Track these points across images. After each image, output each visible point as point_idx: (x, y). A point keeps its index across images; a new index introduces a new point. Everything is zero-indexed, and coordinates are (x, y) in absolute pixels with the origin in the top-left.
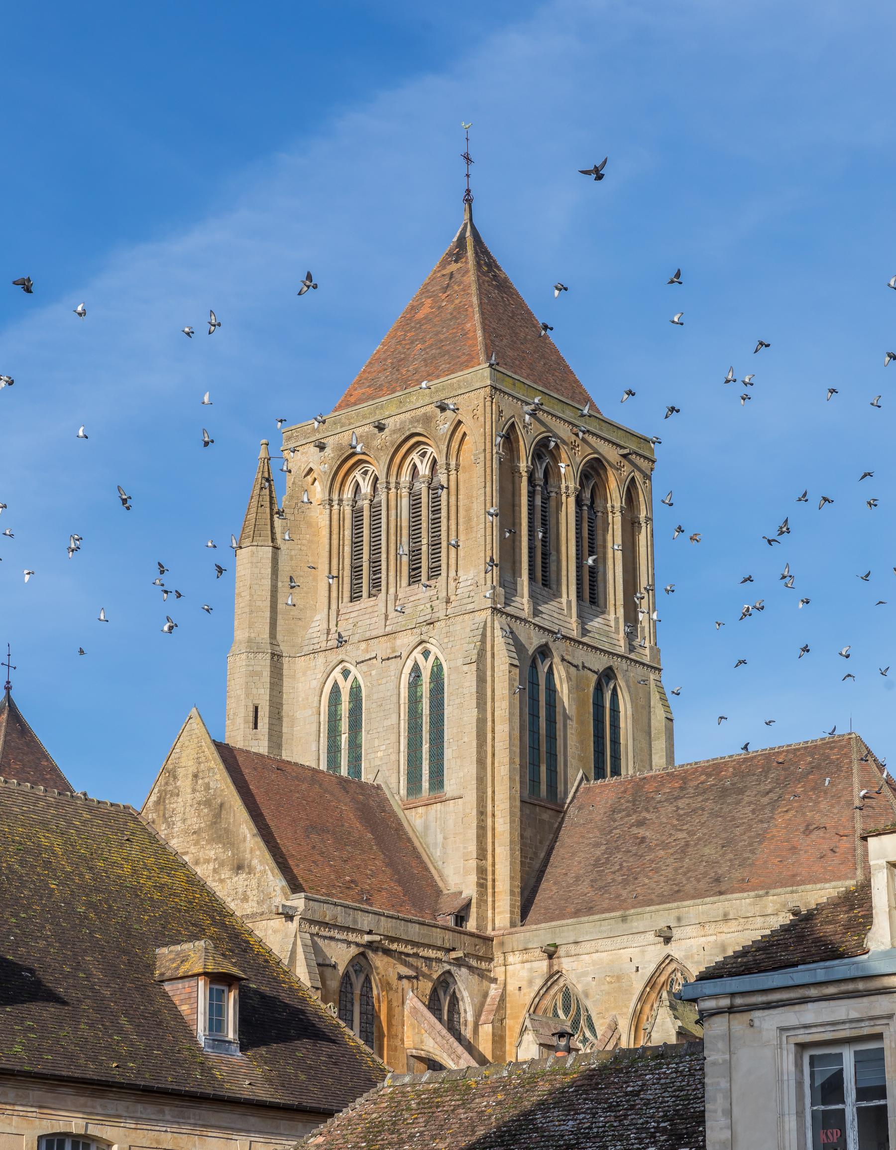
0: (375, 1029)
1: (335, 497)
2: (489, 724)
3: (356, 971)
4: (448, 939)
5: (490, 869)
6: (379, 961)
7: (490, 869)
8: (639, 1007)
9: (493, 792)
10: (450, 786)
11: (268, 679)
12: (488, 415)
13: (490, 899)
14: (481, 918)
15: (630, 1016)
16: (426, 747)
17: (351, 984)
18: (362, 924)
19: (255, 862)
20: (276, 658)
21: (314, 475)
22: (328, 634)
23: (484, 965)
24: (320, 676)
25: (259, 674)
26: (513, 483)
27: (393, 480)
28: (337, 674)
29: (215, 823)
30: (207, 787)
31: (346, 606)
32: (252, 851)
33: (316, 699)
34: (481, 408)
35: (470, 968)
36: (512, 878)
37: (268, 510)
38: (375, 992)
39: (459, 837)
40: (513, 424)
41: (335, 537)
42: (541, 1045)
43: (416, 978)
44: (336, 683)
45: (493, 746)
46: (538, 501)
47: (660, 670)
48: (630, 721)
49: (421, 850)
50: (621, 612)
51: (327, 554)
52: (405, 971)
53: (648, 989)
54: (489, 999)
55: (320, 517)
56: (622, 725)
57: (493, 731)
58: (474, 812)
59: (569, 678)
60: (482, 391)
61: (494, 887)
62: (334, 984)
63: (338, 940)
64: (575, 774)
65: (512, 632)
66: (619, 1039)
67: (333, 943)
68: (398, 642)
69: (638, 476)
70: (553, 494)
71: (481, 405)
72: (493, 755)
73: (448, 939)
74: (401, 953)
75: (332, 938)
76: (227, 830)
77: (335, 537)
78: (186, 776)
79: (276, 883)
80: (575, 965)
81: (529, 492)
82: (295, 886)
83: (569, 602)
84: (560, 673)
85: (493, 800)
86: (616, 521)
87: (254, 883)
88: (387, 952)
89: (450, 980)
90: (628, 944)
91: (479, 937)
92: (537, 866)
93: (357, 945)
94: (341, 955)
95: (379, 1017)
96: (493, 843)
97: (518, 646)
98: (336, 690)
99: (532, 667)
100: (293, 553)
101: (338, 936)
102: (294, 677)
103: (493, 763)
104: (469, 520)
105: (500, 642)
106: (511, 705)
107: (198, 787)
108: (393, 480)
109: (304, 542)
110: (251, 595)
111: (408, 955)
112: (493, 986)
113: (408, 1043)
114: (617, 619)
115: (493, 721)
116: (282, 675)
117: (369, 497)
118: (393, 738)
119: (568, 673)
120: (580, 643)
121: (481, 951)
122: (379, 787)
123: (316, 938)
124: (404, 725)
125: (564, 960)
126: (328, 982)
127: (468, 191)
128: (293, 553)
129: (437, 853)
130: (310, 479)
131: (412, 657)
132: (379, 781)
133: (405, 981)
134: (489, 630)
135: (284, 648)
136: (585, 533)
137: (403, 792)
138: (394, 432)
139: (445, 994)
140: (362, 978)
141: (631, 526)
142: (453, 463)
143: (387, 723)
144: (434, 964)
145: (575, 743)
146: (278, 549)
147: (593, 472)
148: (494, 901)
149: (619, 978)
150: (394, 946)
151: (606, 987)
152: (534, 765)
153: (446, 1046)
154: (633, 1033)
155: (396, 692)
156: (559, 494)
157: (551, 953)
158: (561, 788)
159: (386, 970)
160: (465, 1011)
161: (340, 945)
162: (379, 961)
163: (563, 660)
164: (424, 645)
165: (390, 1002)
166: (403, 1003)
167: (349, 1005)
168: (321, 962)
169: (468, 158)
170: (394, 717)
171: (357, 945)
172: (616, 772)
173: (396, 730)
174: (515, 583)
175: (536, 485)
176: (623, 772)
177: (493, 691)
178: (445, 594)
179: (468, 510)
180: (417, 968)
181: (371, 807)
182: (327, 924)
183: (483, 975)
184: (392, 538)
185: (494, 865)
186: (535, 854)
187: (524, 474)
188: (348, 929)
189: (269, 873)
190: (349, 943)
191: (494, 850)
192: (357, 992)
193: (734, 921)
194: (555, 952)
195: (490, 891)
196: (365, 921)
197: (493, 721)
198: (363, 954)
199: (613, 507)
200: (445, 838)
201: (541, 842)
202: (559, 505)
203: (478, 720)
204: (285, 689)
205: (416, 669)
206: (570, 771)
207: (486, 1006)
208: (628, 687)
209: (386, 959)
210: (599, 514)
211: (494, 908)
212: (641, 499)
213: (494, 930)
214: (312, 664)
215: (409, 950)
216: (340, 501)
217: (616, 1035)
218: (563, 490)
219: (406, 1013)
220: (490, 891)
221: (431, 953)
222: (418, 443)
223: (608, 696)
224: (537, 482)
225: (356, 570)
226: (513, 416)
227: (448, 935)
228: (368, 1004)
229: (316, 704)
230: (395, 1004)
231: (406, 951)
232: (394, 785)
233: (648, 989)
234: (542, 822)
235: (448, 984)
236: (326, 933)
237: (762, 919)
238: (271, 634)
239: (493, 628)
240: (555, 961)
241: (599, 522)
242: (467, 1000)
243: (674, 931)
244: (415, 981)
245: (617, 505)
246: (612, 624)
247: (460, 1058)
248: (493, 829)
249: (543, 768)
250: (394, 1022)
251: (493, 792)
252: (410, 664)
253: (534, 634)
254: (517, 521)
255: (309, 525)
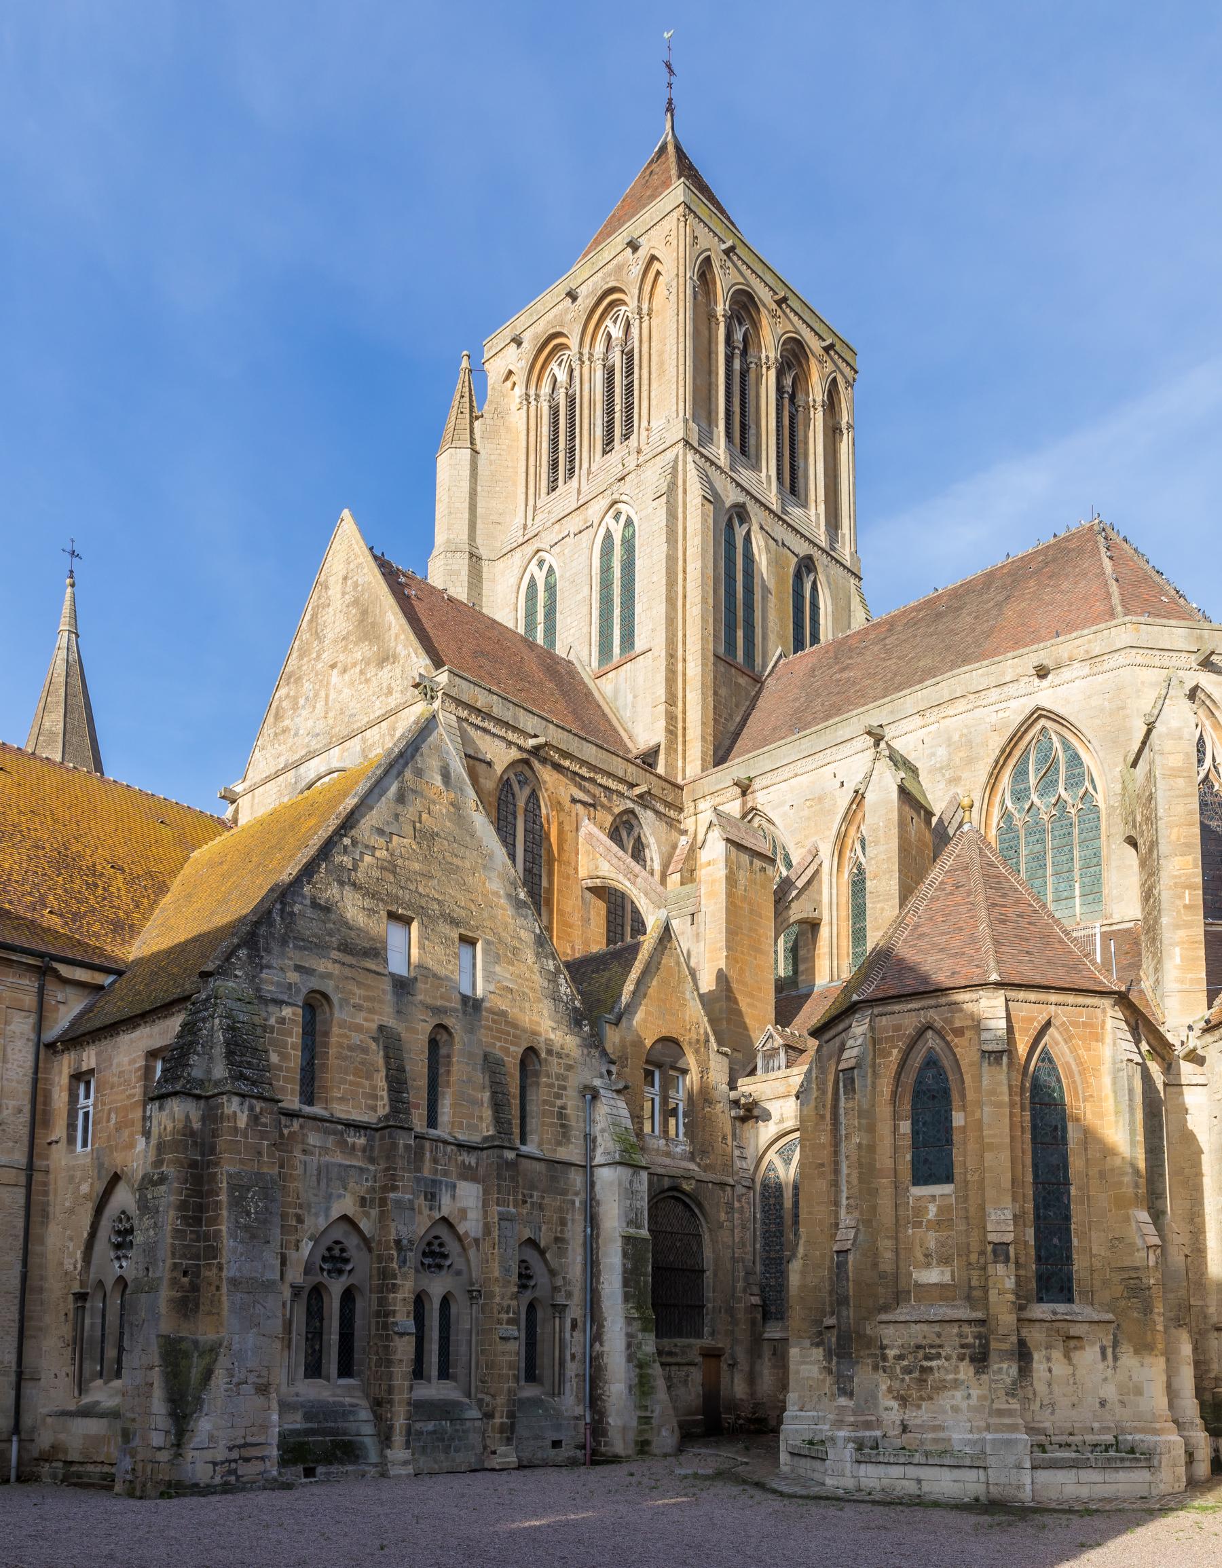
0: (543, 852)
1: (532, 392)
2: (680, 563)
3: (519, 782)
4: (632, 773)
5: (680, 716)
6: (547, 775)
7: (680, 716)
8: (843, 828)
9: (685, 635)
10: (640, 644)
11: (466, 578)
12: (682, 237)
13: (680, 748)
14: (670, 765)
15: (833, 839)
16: (617, 612)
17: (513, 795)
18: (525, 724)
19: (400, 648)
20: (474, 559)
21: (513, 378)
22: (525, 529)
23: (672, 814)
24: (517, 572)
25: (458, 573)
26: (710, 329)
27: (586, 351)
28: (533, 567)
29: (362, 621)
30: (356, 585)
31: (544, 498)
32: (397, 636)
33: (514, 595)
34: (674, 233)
35: (657, 812)
36: (703, 723)
37: (468, 416)
38: (544, 811)
39: (648, 695)
40: (708, 258)
41: (532, 433)
42: (728, 840)
43: (593, 806)
44: (532, 576)
45: (685, 587)
46: (737, 365)
47: (861, 579)
48: (830, 618)
49: (611, 716)
50: (822, 508)
51: (524, 451)
52: (580, 795)
53: (854, 806)
54: (678, 852)
55: (518, 419)
56: (822, 621)
57: (685, 572)
58: (664, 653)
59: (768, 551)
60: (675, 214)
61: (684, 736)
62: (489, 784)
63: (494, 735)
64: (774, 646)
65: (707, 476)
66: (820, 865)
67: (488, 738)
68: (590, 511)
69: (840, 380)
70: (753, 365)
71: (674, 228)
72: (685, 597)
73: (632, 773)
74: (575, 773)
75: (485, 730)
76: (373, 625)
77: (532, 433)
78: (337, 582)
79: (419, 663)
80: (770, 798)
81: (726, 354)
82: (438, 663)
83: (768, 477)
84: (758, 543)
85: (684, 643)
86: (818, 418)
87: (398, 671)
88: (557, 767)
89: (634, 822)
90: (832, 759)
91: (666, 780)
92: (732, 729)
93: (520, 748)
94: (500, 755)
95: (548, 838)
96: (684, 689)
97: (712, 498)
98: (532, 584)
99: (729, 522)
100: (492, 457)
101: (494, 730)
102: (493, 580)
103: (684, 605)
104: (661, 363)
105: (692, 473)
106: (704, 541)
107: (348, 590)
108: (586, 351)
109: (504, 447)
110: (450, 497)
111: (583, 778)
112: (683, 838)
113: (583, 872)
114: (817, 515)
115: (685, 561)
116: (481, 577)
117: (565, 385)
118: (585, 610)
119: (766, 543)
120: (780, 518)
121: (667, 800)
122: (569, 662)
123: (465, 725)
124: (596, 596)
125: (757, 794)
126: (482, 780)
127: (670, 100)
128: (492, 457)
129: (626, 714)
130: (509, 384)
131: (604, 524)
132: (572, 657)
133: (579, 806)
134: (680, 464)
135: (483, 552)
136: (786, 422)
137: (595, 664)
138: (587, 297)
139: (628, 835)
140: (527, 791)
141: (833, 432)
142: (645, 307)
143: (579, 597)
144: (615, 797)
145: (774, 619)
146: (477, 452)
147: (794, 356)
148: (684, 751)
149: (820, 799)
150: (566, 763)
151: (806, 813)
152: (731, 628)
153: (623, 867)
154: (836, 859)
155: (588, 562)
156: (759, 366)
157: (745, 788)
158: (758, 660)
159: (556, 788)
160: (652, 859)
161: (497, 741)
162: (547, 775)
163: (762, 528)
164: (616, 506)
165: (560, 824)
166: (577, 830)
167: (510, 817)
168: (471, 752)
169: (669, 66)
170: (586, 589)
171: (520, 748)
172: (815, 639)
173: (588, 602)
174: (711, 433)
175: (734, 348)
176: (822, 637)
177: (685, 529)
178: (636, 444)
179: (661, 354)
180: (594, 796)
181: (560, 675)
182: (480, 711)
183: (673, 824)
184: (586, 412)
185: (684, 712)
186: (731, 715)
187: (721, 319)
188: (506, 725)
189: (413, 655)
190: (510, 743)
191: (684, 697)
192: (521, 803)
193: (961, 700)
194: (749, 786)
195: (680, 739)
196: (529, 723)
197: (685, 561)
198: (526, 762)
199: (814, 401)
200: (635, 697)
201: (737, 706)
202: (759, 377)
203: (668, 556)
204: (484, 592)
205: (608, 536)
206: (770, 645)
207: (675, 858)
208: (829, 583)
209: (556, 775)
210: (801, 409)
211: (684, 758)
212: (843, 405)
213: (684, 779)
214: (510, 562)
215: (584, 771)
216: (537, 396)
217: (817, 861)
218: (764, 360)
219: (581, 840)
220: (680, 739)
221: (613, 785)
222: (612, 305)
223: (808, 586)
224: (736, 344)
225: (554, 466)
226: (709, 250)
227: (631, 769)
228: (534, 822)
229: (513, 600)
230: (567, 828)
231: (580, 772)
232: (585, 659)
233: (854, 806)
234: (738, 685)
235: (632, 826)
236: (478, 722)
237: (998, 690)
238: (469, 535)
239: (685, 463)
240: (749, 797)
241: (800, 417)
242: (654, 847)
243: (886, 729)
244: (592, 809)
245: (819, 399)
246: (813, 519)
247: (637, 876)
248: (684, 675)
249: (740, 634)
250: (566, 847)
251: (685, 635)
252: (602, 531)
253: (731, 487)
254: (713, 368)
255: (508, 429)
